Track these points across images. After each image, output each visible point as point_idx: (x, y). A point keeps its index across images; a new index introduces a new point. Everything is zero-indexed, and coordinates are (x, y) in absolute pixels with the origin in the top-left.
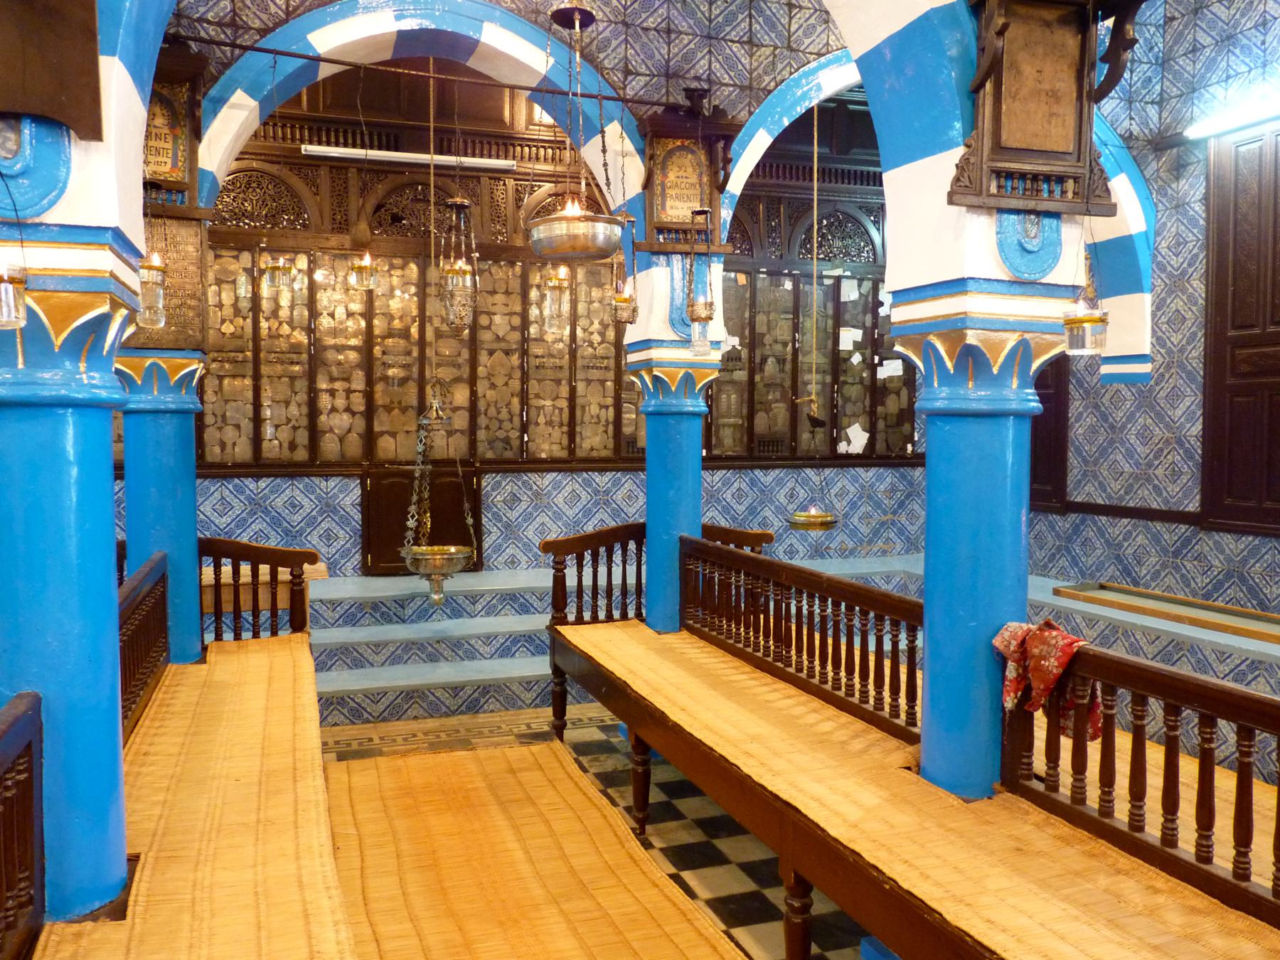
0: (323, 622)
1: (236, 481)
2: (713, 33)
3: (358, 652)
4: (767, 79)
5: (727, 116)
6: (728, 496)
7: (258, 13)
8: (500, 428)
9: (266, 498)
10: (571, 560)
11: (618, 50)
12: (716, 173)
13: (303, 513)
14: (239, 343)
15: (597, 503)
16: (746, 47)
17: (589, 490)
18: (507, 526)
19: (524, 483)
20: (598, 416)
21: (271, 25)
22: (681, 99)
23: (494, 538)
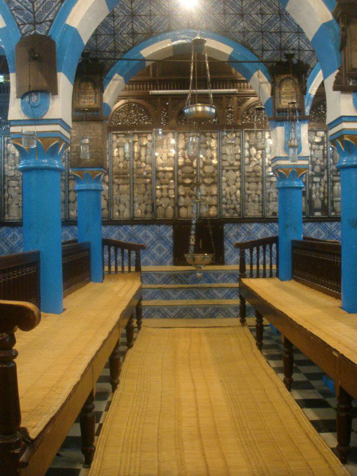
0: (155, 282)
8: (232, 204)
10: (247, 251)
12: (302, 87)
14: (125, 171)
17: (273, 231)
22: (284, 60)
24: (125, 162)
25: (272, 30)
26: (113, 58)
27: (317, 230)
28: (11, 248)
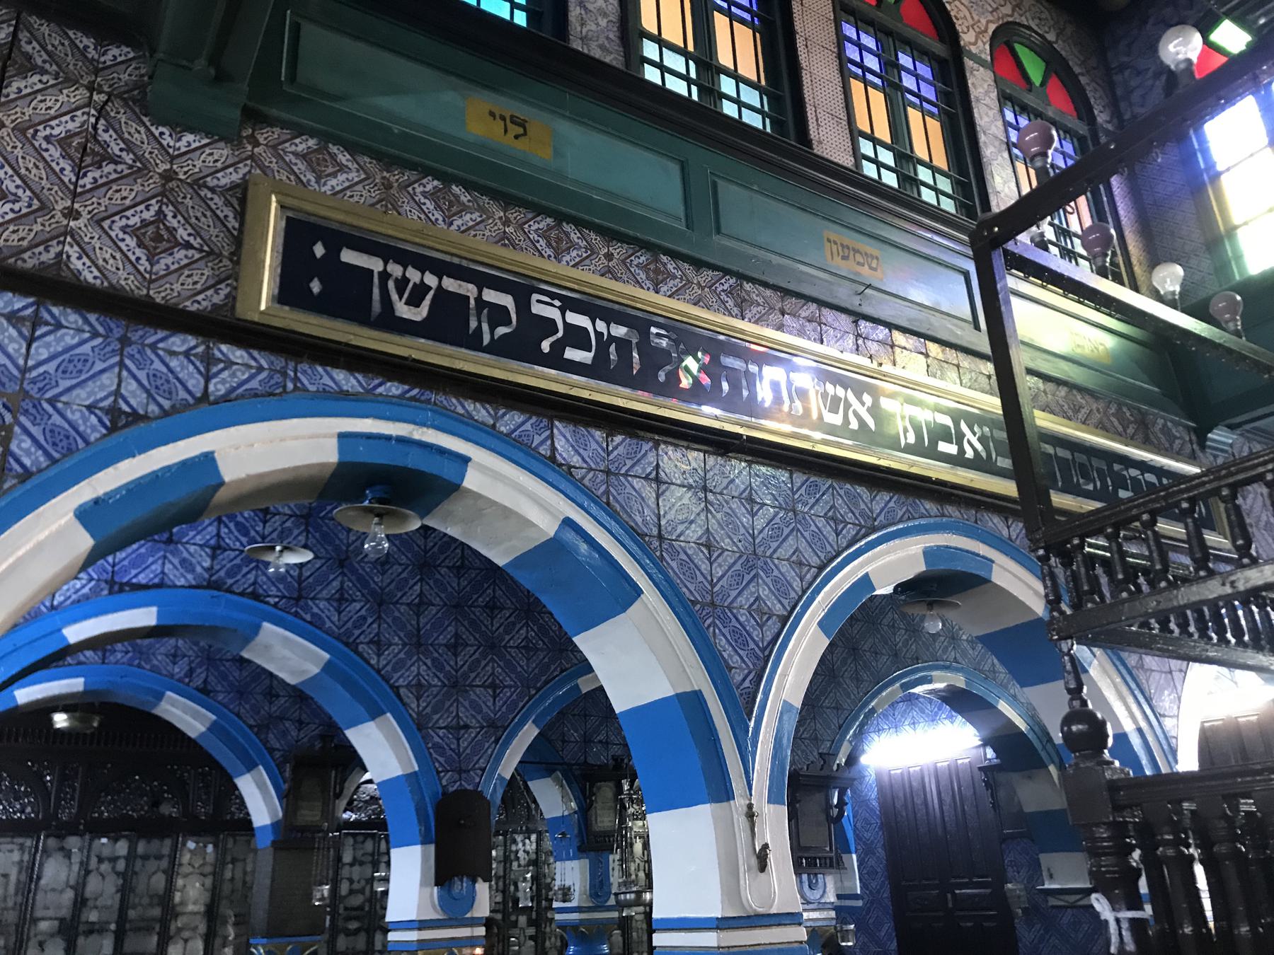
5: (215, 721)
25: (499, 593)
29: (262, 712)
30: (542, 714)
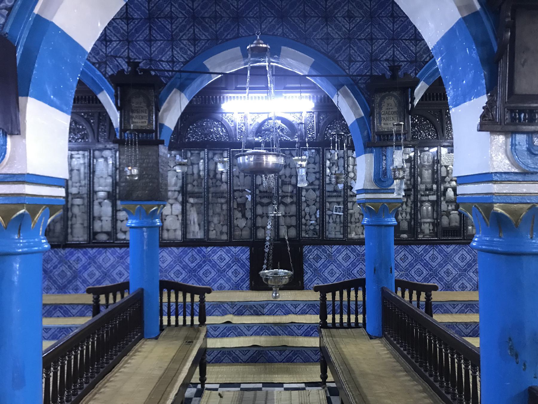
1: (198, 248)
2: (395, 38)
3: (240, 329)
4: (425, 56)
6: (427, 258)
7: (183, 55)
9: (210, 256)
11: (346, 51)
13: (225, 262)
15: (358, 261)
16: (413, 42)
18: (315, 270)
19: (323, 250)
20: (358, 219)
21: (188, 59)
23: (309, 276)
24: (199, 181)
26: (171, 69)
27: (403, 253)
28: (74, 272)
29: (101, 53)
30: (429, 77)
